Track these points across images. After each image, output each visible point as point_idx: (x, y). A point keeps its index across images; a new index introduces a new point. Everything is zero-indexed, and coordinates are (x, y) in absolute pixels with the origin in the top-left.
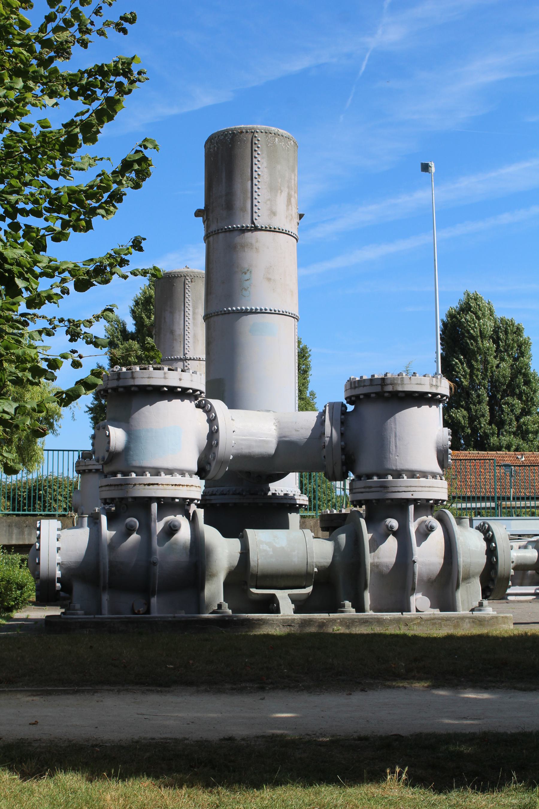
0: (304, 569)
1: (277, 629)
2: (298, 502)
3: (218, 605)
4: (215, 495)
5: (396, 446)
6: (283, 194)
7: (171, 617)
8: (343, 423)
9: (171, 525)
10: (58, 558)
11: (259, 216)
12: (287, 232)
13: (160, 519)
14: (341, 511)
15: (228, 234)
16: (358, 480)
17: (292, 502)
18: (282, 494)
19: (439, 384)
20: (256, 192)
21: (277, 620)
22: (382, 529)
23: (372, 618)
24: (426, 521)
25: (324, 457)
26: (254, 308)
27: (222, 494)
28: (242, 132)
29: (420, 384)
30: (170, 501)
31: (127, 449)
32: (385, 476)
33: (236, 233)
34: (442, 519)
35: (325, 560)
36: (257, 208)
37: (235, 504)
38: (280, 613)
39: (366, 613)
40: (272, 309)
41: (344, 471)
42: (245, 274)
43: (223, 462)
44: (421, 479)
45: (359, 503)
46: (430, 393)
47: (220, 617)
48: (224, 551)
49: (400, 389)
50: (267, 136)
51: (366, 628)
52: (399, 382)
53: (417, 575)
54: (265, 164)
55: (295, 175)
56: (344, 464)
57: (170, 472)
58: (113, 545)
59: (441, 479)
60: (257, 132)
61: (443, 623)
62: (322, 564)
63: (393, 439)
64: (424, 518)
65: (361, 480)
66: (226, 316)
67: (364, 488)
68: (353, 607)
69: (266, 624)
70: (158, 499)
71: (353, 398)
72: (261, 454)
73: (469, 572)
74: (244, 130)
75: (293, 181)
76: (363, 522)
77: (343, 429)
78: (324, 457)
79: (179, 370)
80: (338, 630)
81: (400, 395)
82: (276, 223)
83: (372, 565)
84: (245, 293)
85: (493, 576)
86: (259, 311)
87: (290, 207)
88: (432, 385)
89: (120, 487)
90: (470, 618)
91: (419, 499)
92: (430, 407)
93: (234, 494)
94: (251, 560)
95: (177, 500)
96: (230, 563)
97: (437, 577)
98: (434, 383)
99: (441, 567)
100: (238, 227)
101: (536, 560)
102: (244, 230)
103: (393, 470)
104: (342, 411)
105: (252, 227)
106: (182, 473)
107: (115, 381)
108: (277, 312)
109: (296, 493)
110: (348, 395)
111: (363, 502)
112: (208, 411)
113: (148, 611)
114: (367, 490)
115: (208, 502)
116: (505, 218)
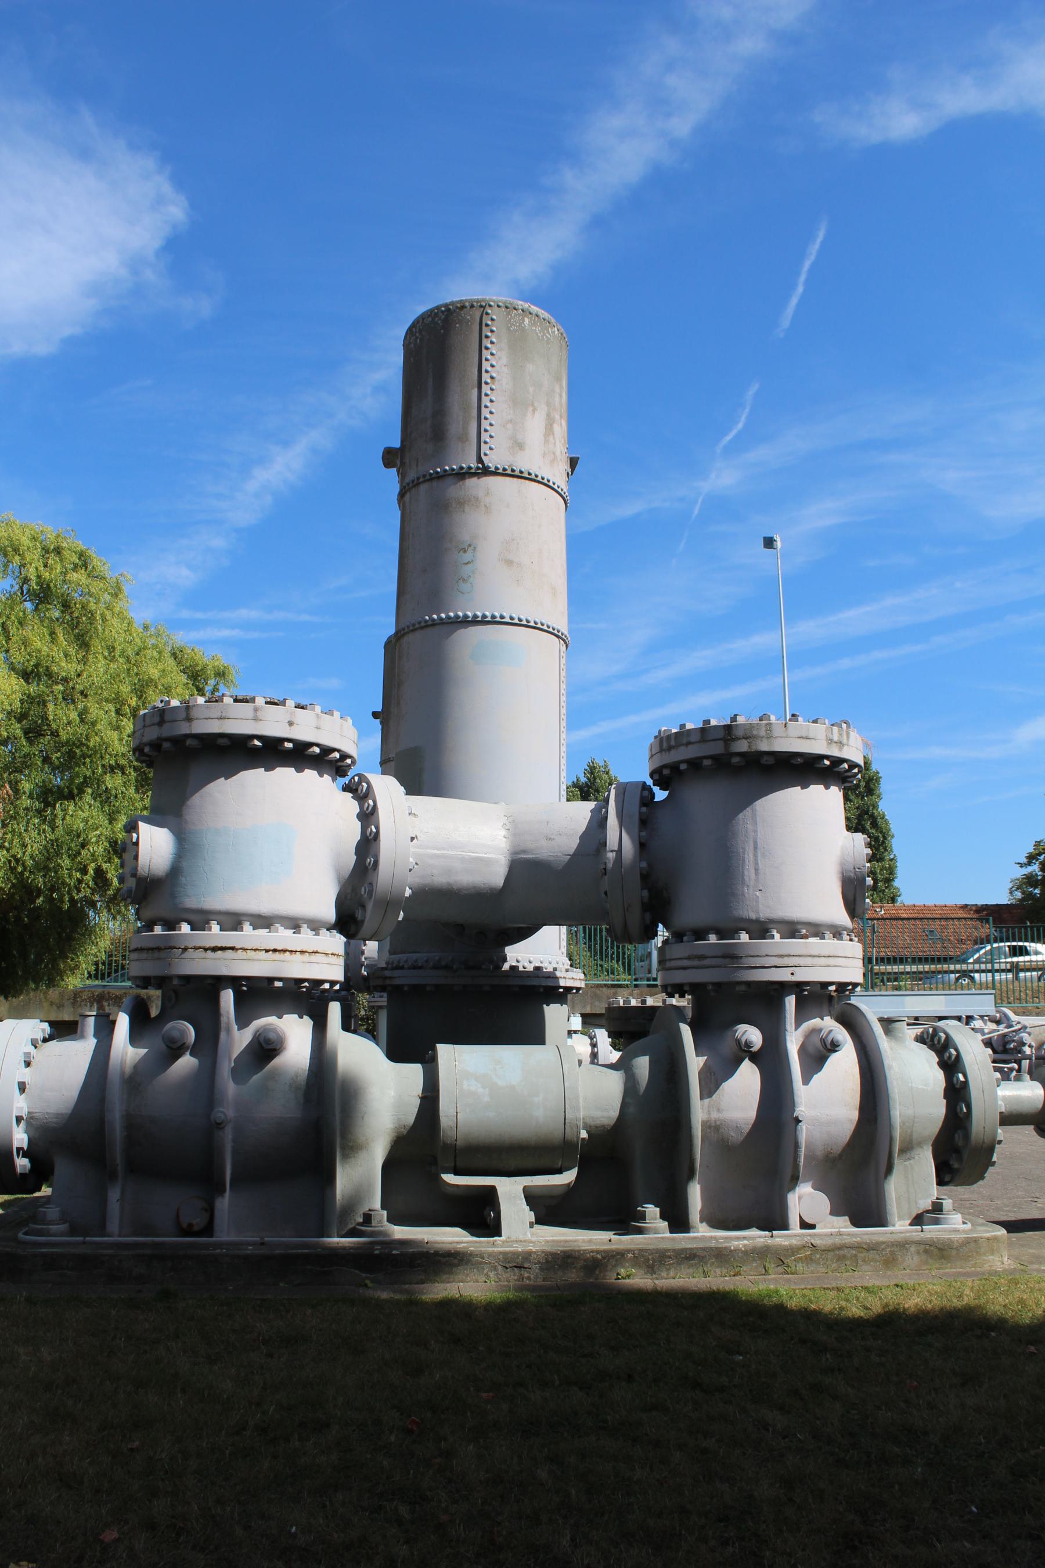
0: (557, 1134)
1: (492, 1274)
2: (562, 983)
3: (364, 1214)
4: (402, 968)
5: (756, 870)
6: (537, 414)
7: (254, 1244)
8: (644, 822)
9: (261, 1039)
10: (21, 1105)
11: (491, 449)
12: (545, 481)
13: (243, 1022)
14: (644, 1002)
15: (435, 483)
16: (676, 942)
17: (550, 983)
18: (530, 968)
19: (845, 741)
20: (486, 407)
21: (490, 1255)
22: (727, 1047)
23: (704, 1249)
24: (820, 1030)
25: (606, 893)
26: (479, 614)
27: (415, 967)
28: (463, 307)
29: (807, 738)
30: (265, 984)
31: (175, 871)
32: (733, 933)
33: (449, 480)
34: (851, 1021)
35: (605, 1114)
36: (488, 434)
37: (437, 986)
38: (500, 1235)
39: (691, 1235)
40: (514, 615)
41: (648, 922)
42: (465, 552)
43: (390, 903)
44: (811, 940)
45: (678, 989)
46: (827, 757)
47: (365, 1243)
48: (384, 1088)
49: (764, 747)
50: (508, 314)
51: (691, 1270)
52: (763, 733)
53: (803, 1149)
54: (504, 360)
55: (561, 387)
56: (646, 907)
57: (263, 922)
58: (136, 1081)
59: (851, 940)
60: (490, 306)
61: (860, 1255)
62: (598, 1122)
63: (751, 856)
64: (815, 1022)
65: (682, 941)
66: (429, 630)
67: (689, 958)
68: (663, 1216)
69: (466, 1263)
70: (234, 982)
71: (666, 772)
72: (474, 888)
73: (911, 1135)
74: (467, 304)
75: (557, 399)
76: (686, 1030)
77: (643, 834)
78: (606, 893)
79: (290, 703)
80: (629, 1276)
81: (765, 760)
82: (523, 463)
83: (706, 1125)
84: (463, 586)
85: (960, 1143)
86: (489, 619)
87: (551, 438)
88: (830, 741)
89: (156, 954)
90: (918, 1243)
91: (807, 983)
92: (827, 787)
93: (435, 967)
94: (442, 1113)
95: (278, 984)
96: (399, 1119)
97: (844, 1150)
98: (836, 738)
99: (852, 1127)
100: (453, 470)
101: (1040, 1105)
102: (463, 474)
103: (751, 921)
104: (642, 798)
105: (478, 468)
106: (295, 924)
108: (524, 622)
109: (560, 966)
110: (657, 765)
111: (686, 988)
112: (359, 791)
113: (208, 1229)
114: (696, 963)
115: (388, 982)
116: (845, 663)
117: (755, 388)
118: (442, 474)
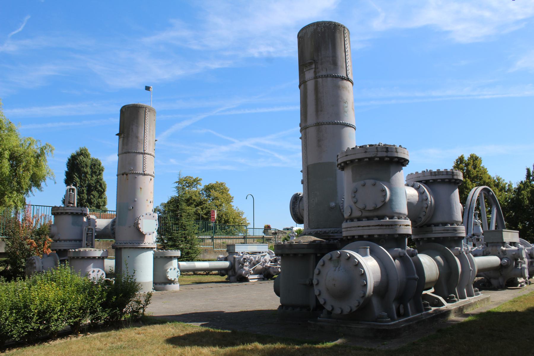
15: (334, 79)
33: (339, 79)
89: (391, 227)
102: (343, 79)
117: (28, 17)
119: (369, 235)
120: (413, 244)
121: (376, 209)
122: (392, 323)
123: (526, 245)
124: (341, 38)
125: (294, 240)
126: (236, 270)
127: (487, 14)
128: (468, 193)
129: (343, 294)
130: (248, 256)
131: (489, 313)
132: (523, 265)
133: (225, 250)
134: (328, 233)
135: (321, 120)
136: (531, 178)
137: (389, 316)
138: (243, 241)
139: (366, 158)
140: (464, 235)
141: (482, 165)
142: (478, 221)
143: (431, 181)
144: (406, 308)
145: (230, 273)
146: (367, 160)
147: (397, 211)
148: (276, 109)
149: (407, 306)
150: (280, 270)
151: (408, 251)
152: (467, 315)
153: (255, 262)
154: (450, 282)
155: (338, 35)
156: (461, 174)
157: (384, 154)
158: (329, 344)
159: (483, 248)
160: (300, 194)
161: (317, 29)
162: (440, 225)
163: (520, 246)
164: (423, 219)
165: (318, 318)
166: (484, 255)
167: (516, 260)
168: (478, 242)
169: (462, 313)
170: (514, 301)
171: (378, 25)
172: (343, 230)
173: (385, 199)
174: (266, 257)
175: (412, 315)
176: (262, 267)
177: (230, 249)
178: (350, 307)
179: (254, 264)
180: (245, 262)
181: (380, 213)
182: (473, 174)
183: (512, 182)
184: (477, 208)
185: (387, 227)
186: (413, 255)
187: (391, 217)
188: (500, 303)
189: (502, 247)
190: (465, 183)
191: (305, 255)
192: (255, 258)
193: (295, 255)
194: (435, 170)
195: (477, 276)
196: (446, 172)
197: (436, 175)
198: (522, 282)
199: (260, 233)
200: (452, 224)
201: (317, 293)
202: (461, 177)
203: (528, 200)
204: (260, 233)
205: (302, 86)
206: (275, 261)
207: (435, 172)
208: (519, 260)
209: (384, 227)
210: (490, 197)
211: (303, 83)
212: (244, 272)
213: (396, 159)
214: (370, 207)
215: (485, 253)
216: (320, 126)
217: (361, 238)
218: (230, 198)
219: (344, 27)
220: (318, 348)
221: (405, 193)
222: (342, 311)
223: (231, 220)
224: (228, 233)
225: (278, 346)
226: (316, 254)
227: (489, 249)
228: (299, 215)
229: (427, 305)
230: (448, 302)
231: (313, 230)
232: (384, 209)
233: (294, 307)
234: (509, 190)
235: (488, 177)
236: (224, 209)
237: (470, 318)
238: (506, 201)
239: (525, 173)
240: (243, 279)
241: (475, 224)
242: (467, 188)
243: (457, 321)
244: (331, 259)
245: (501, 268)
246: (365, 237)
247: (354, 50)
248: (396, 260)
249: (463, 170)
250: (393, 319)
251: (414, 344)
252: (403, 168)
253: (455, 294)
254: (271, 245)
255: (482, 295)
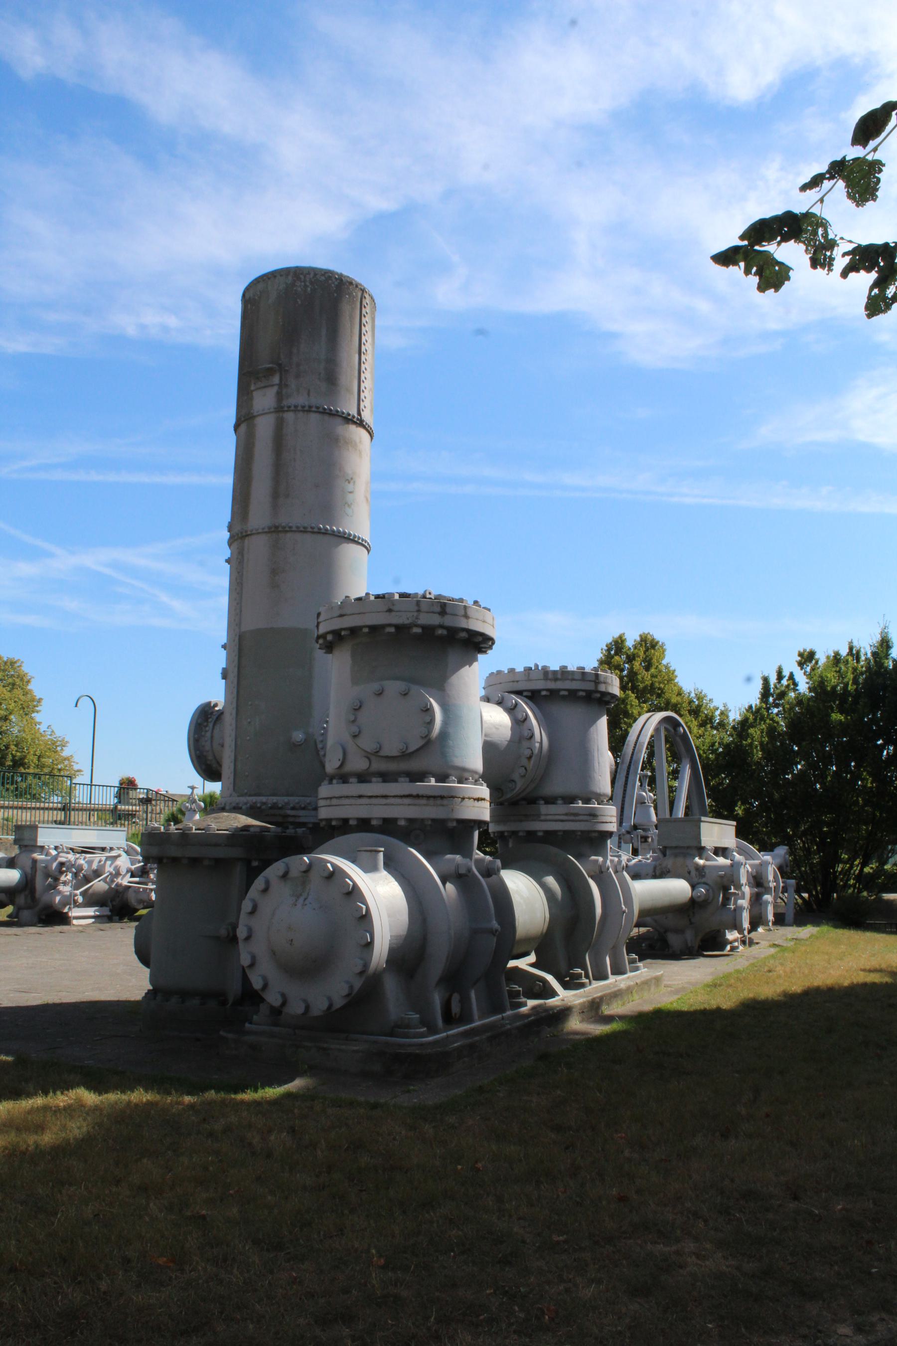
4: (304, 809)
15: (326, 417)
33: (339, 420)
66: (320, 537)
67: (566, 814)
89: (439, 802)
102: (348, 420)
107: (437, 615)
118: (334, 412)
119: (385, 820)
120: (493, 843)
121: (405, 755)
122: (431, 1038)
123: (748, 856)
124: (352, 318)
125: (195, 821)
126: (38, 894)
127: (703, 306)
128: (630, 726)
129: (311, 966)
130: (71, 857)
131: (658, 1014)
132: (740, 902)
133: (11, 838)
134: (281, 808)
135: (283, 520)
136: (771, 699)
137: (423, 1022)
138: (60, 816)
139: (390, 625)
140: (613, 827)
141: (664, 662)
142: (649, 795)
143: (544, 693)
144: (465, 1001)
145: (21, 900)
146: (392, 630)
147: (458, 762)
148: (173, 479)
149: (469, 998)
150: (153, 896)
151: (479, 862)
152: (609, 1019)
153: (90, 873)
154: (571, 940)
155: (345, 307)
156: (616, 682)
157: (435, 620)
158: (272, 1092)
159: (655, 859)
160: (216, 705)
161: (293, 284)
162: (560, 802)
163: (738, 857)
164: (520, 784)
165: (247, 1025)
166: (655, 876)
167: (726, 889)
168: (645, 845)
169: (597, 1013)
170: (715, 985)
171: (449, 294)
172: (321, 803)
173: (430, 731)
174: (118, 862)
175: (480, 1018)
176: (106, 887)
177: (25, 837)
178: (329, 999)
179: (87, 880)
180: (62, 873)
181: (414, 765)
182: (643, 682)
183: (730, 706)
184: (648, 764)
185: (431, 801)
186: (489, 872)
187: (442, 778)
188: (683, 989)
189: (697, 859)
190: (624, 701)
191: (220, 864)
192: (90, 863)
193: (195, 862)
194: (555, 667)
195: (638, 925)
196: (582, 674)
197: (556, 680)
198: (736, 940)
199: (108, 799)
200: (587, 801)
201: (245, 960)
202: (616, 690)
203: (762, 750)
204: (108, 799)
205: (243, 427)
206: (143, 873)
207: (555, 672)
208: (732, 890)
209: (424, 801)
210: (678, 739)
211: (245, 419)
212: (58, 899)
213: (464, 635)
214: (392, 748)
215: (658, 874)
216: (281, 535)
217: (364, 825)
218: (33, 700)
219: (363, 291)
220: (242, 1102)
221: (479, 719)
222: (307, 1008)
223: (31, 759)
224: (19, 794)
225: (139, 1096)
226: (248, 862)
227: (669, 862)
228: (210, 758)
229: (517, 994)
230: (566, 986)
231: (243, 799)
232: (423, 757)
233: (184, 995)
234: (722, 725)
235: (676, 692)
236: (15, 730)
237: (615, 1026)
238: (714, 752)
239: (758, 686)
240: (54, 917)
241: (641, 802)
242: (627, 714)
243: (583, 1034)
244: (285, 876)
245: (692, 906)
246: (374, 822)
247: (383, 349)
248: (448, 885)
249: (622, 670)
250: (433, 1030)
251: (481, 1090)
252: (480, 656)
253: (584, 968)
254: (133, 829)
255: (646, 970)
